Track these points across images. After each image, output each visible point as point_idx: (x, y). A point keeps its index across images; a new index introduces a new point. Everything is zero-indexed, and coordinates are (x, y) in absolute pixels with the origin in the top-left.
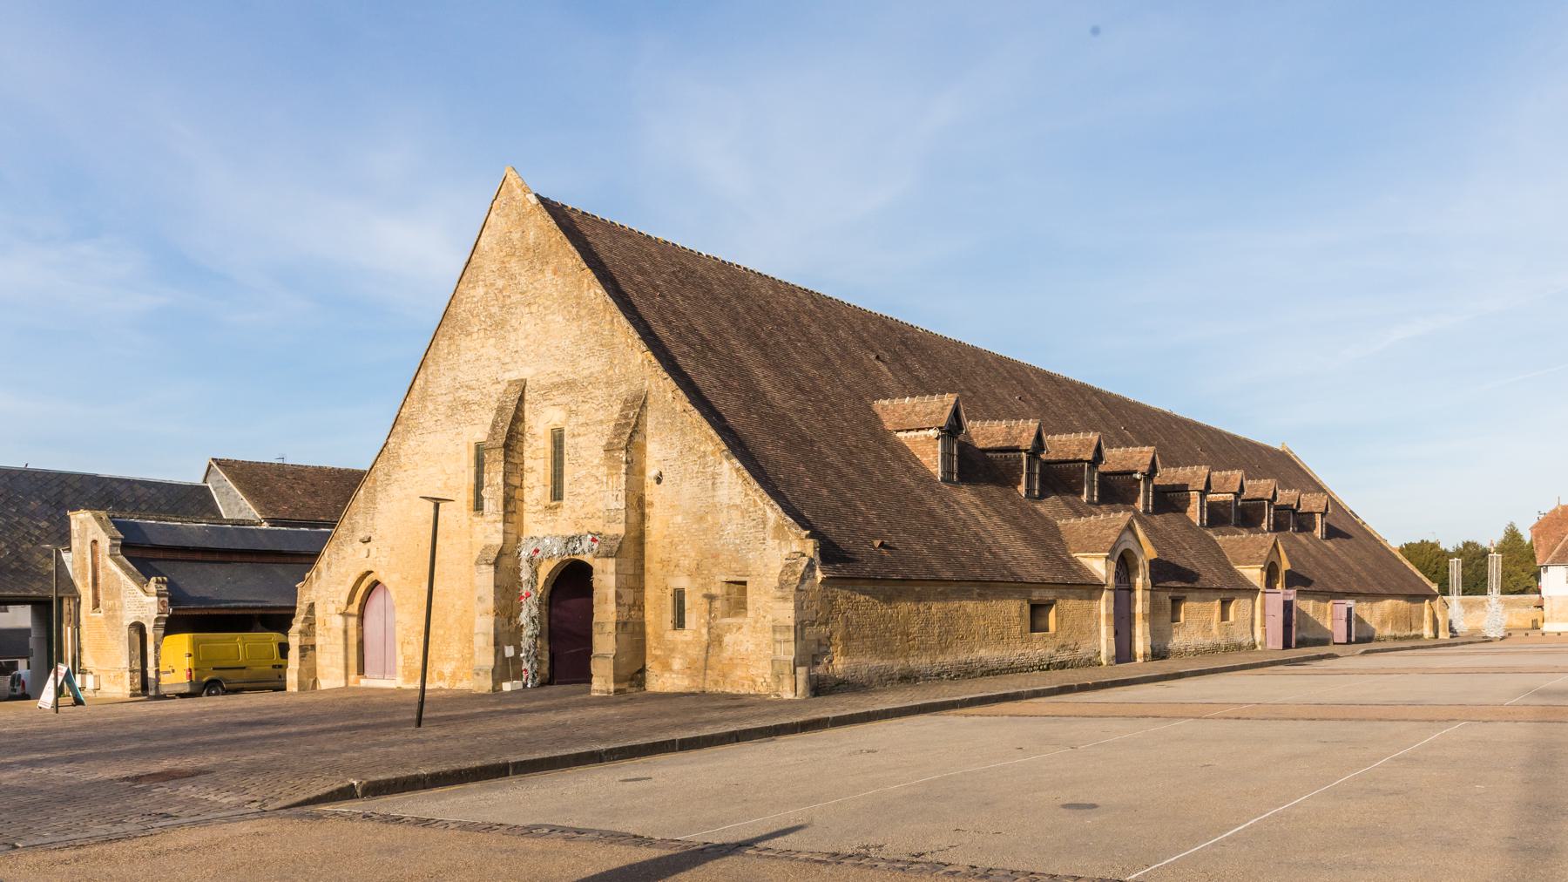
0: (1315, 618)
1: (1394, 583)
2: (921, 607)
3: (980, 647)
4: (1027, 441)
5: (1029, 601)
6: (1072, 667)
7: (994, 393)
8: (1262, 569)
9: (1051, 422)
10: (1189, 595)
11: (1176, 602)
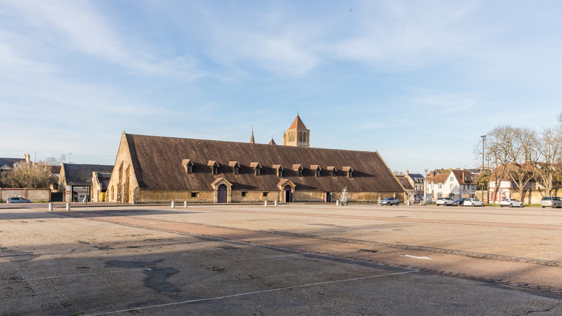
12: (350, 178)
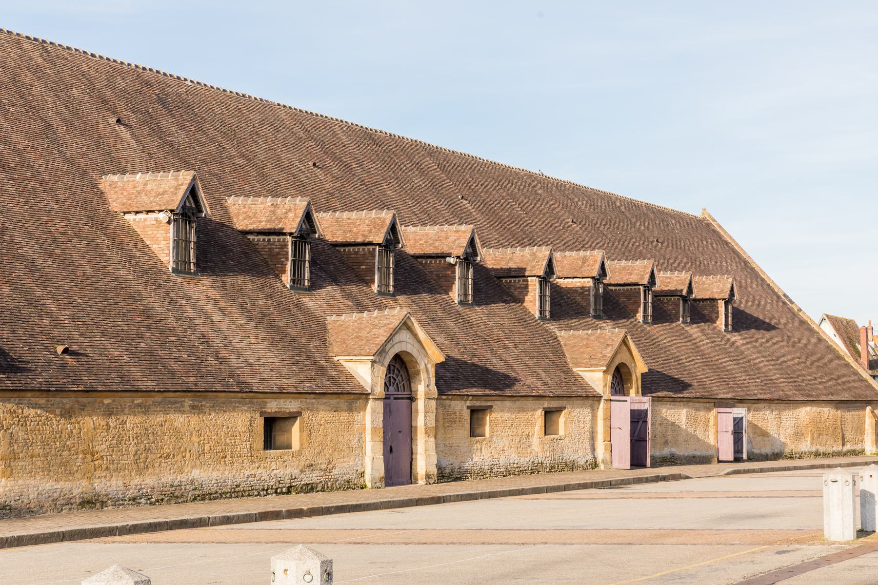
0: (691, 430)
1: (821, 387)
2: (112, 421)
3: (192, 467)
4: (292, 224)
5: (261, 414)
6: (323, 490)
7: (279, 159)
8: (605, 372)
9: (353, 193)
10: (497, 404)
11: (477, 414)
12: (388, 294)
